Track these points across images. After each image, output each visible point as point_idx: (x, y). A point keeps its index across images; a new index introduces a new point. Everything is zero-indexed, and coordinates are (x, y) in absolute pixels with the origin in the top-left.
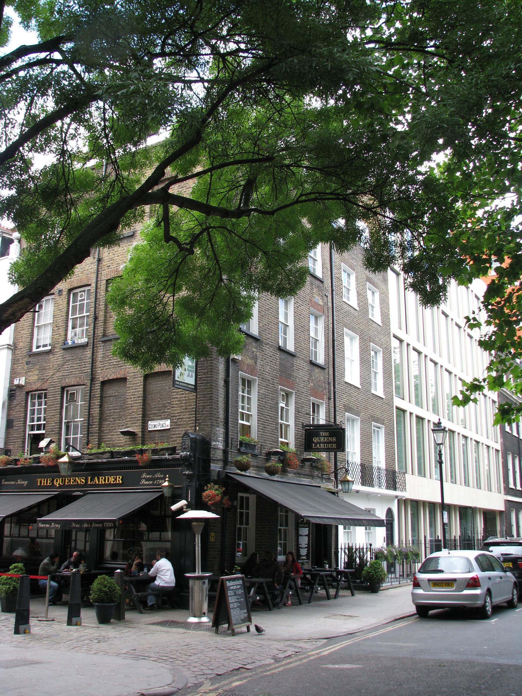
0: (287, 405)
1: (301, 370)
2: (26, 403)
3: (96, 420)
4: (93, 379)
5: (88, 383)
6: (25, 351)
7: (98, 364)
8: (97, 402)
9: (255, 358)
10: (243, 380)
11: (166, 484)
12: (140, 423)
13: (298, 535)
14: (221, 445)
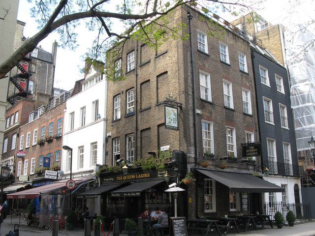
0: (231, 135)
1: (239, 118)
2: (113, 143)
3: (139, 149)
4: (137, 130)
5: (135, 131)
6: (111, 120)
7: (139, 123)
8: (139, 140)
9: (211, 113)
10: (247, 134)
11: (166, 175)
12: (157, 148)
13: (241, 198)
14: (193, 156)
